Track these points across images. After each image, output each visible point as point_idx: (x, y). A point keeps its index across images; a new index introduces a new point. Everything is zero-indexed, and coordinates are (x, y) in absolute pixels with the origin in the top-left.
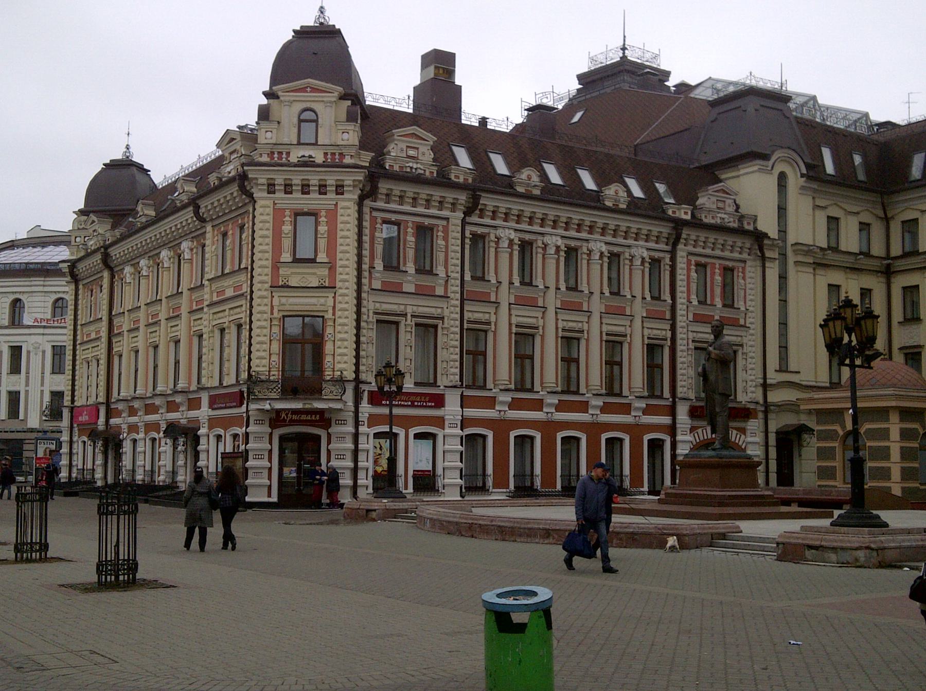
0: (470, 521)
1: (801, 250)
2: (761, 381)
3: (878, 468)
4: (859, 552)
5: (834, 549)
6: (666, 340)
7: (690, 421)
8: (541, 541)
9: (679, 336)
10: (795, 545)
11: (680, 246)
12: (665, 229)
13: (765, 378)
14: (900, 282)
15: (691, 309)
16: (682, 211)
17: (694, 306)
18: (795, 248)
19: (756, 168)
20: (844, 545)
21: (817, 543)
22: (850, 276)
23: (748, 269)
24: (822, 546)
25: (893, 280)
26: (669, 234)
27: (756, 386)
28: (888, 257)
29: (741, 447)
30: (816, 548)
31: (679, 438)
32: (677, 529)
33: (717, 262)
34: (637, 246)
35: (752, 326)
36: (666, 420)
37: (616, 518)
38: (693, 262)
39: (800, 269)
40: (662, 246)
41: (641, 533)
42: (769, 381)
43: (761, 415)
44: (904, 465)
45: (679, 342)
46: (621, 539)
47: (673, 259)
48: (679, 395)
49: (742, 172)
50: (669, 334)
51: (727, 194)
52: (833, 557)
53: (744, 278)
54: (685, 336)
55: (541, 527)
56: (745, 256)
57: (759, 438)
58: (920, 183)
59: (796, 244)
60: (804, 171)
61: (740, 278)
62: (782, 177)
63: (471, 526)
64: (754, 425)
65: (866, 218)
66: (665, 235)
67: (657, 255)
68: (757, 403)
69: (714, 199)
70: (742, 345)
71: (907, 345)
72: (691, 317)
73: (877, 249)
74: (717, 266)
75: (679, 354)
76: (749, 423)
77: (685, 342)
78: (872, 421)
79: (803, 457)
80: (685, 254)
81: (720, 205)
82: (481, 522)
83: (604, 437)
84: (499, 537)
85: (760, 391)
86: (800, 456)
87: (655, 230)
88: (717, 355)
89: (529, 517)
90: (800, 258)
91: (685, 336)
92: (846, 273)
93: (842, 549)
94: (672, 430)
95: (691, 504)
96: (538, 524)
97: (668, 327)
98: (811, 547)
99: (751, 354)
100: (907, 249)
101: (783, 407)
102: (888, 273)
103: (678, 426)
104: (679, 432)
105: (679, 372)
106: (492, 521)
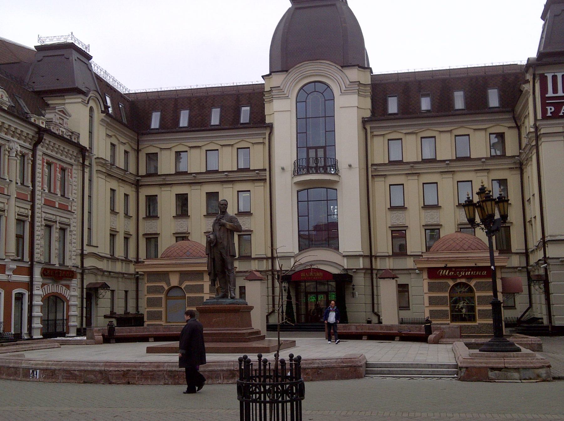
0: (125, 369)
1: (101, 163)
2: (80, 252)
3: (483, 310)
4: (540, 370)
5: (517, 369)
6: (27, 217)
7: (41, 280)
8: (225, 381)
9: (37, 215)
10: (480, 368)
11: (39, 147)
12: (30, 132)
13: (82, 249)
14: (145, 192)
15: (44, 195)
16: (41, 121)
17: (45, 193)
18: (98, 161)
19: (80, 100)
20: (528, 365)
21: (502, 365)
22: (121, 185)
23: (74, 171)
24: (505, 368)
25: (140, 190)
26: (33, 136)
27: (76, 255)
28: (137, 175)
29: (67, 298)
30: (500, 369)
31: (35, 292)
32: (353, 362)
33: (58, 163)
34: (14, 142)
35: (76, 212)
36: (25, 278)
37: (210, 357)
38: (45, 161)
39: (100, 175)
40: (27, 145)
41: (328, 368)
42: (85, 252)
43: (79, 276)
44: (432, 308)
45: (37, 219)
46: (307, 374)
47: (34, 156)
48: (36, 260)
49: (67, 101)
50: (30, 213)
51: (65, 114)
52: (516, 375)
53: (71, 178)
54: (40, 215)
55: (224, 368)
56: (72, 161)
57: (77, 293)
58: (397, 116)
59: (97, 158)
60: (103, 109)
61: (70, 177)
62: (91, 108)
63: (125, 374)
64: (75, 283)
65: (128, 149)
66: (30, 137)
67: (24, 151)
68: (77, 267)
69: (58, 116)
70: (69, 225)
71: (148, 232)
72: (43, 202)
73: (132, 169)
74: (58, 166)
75: (36, 228)
76: (73, 282)
77: (40, 219)
78: (191, 280)
79: (99, 306)
80: (41, 153)
81: (61, 121)
82: (141, 368)
83: (15, 292)
84: (171, 381)
85: (79, 258)
86: (97, 304)
87: (26, 131)
88: (231, 226)
89: (406, 361)
90: (100, 168)
91: (40, 215)
92: (119, 182)
93: (525, 368)
94: (30, 286)
95: (216, 341)
96: (222, 366)
97: (29, 207)
98: (493, 369)
99: (74, 232)
100: (242, 166)
101: (96, 271)
102: (137, 185)
103: (34, 283)
104: (35, 287)
105: (36, 242)
106: (158, 367)
